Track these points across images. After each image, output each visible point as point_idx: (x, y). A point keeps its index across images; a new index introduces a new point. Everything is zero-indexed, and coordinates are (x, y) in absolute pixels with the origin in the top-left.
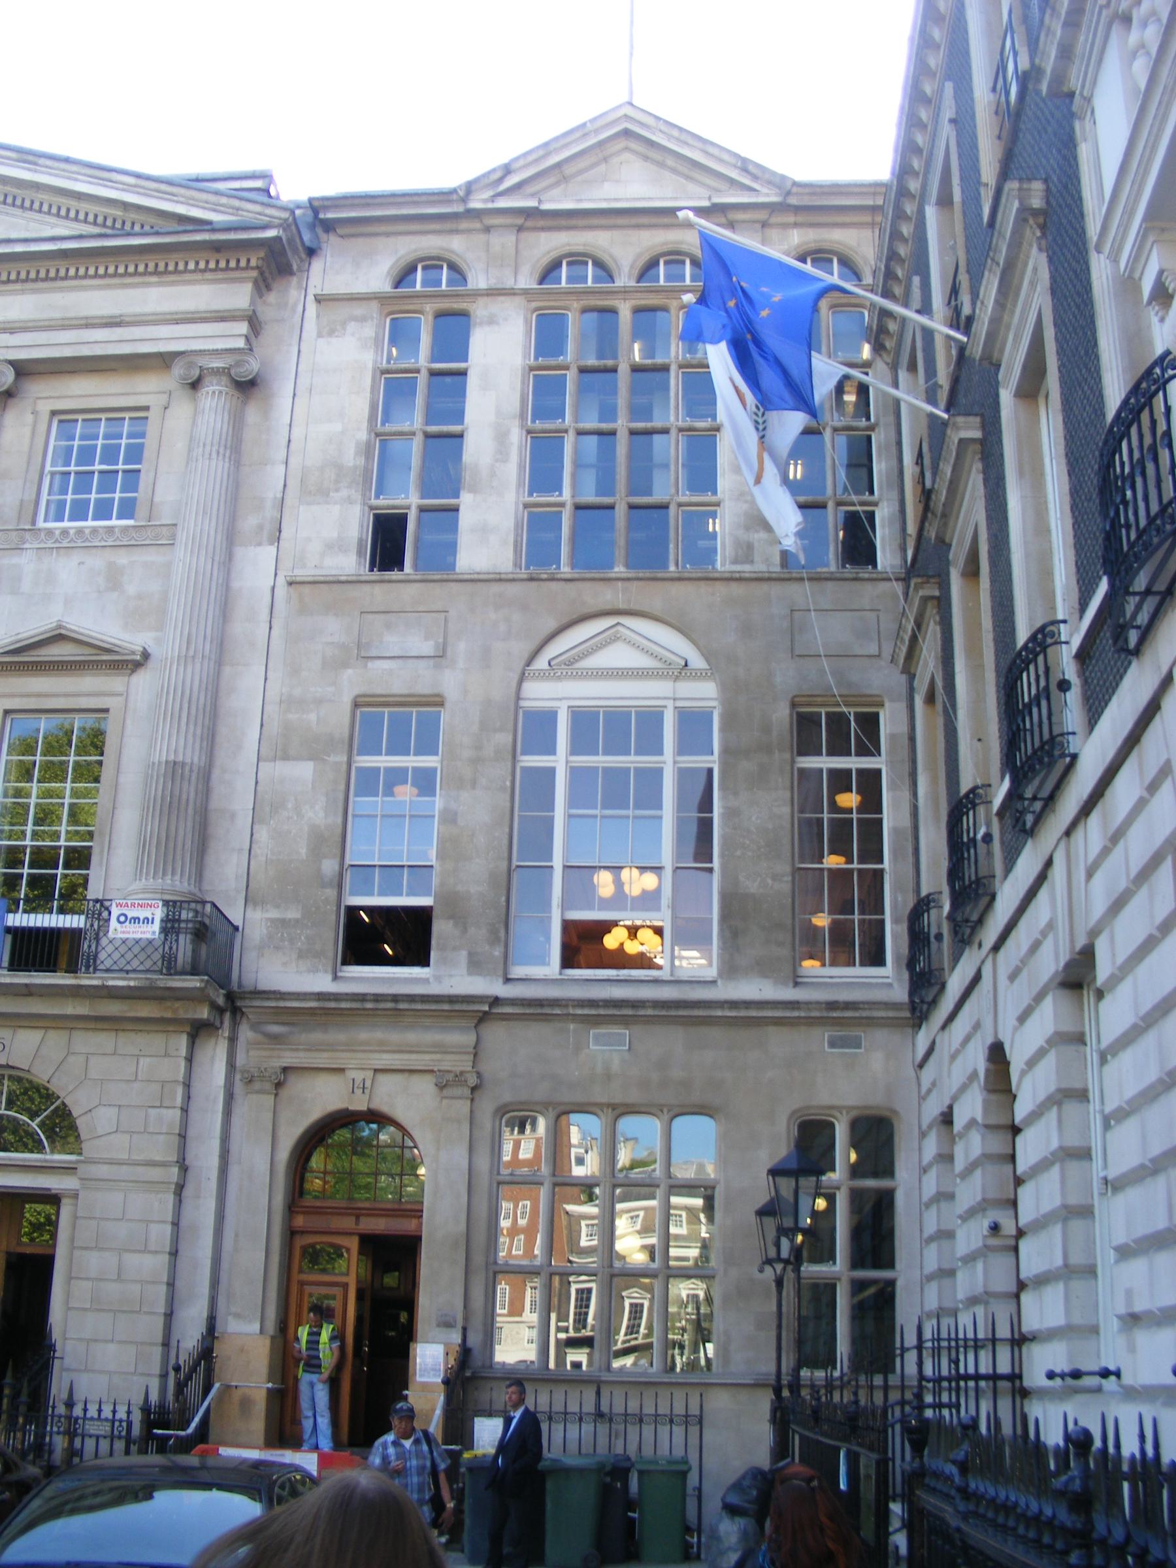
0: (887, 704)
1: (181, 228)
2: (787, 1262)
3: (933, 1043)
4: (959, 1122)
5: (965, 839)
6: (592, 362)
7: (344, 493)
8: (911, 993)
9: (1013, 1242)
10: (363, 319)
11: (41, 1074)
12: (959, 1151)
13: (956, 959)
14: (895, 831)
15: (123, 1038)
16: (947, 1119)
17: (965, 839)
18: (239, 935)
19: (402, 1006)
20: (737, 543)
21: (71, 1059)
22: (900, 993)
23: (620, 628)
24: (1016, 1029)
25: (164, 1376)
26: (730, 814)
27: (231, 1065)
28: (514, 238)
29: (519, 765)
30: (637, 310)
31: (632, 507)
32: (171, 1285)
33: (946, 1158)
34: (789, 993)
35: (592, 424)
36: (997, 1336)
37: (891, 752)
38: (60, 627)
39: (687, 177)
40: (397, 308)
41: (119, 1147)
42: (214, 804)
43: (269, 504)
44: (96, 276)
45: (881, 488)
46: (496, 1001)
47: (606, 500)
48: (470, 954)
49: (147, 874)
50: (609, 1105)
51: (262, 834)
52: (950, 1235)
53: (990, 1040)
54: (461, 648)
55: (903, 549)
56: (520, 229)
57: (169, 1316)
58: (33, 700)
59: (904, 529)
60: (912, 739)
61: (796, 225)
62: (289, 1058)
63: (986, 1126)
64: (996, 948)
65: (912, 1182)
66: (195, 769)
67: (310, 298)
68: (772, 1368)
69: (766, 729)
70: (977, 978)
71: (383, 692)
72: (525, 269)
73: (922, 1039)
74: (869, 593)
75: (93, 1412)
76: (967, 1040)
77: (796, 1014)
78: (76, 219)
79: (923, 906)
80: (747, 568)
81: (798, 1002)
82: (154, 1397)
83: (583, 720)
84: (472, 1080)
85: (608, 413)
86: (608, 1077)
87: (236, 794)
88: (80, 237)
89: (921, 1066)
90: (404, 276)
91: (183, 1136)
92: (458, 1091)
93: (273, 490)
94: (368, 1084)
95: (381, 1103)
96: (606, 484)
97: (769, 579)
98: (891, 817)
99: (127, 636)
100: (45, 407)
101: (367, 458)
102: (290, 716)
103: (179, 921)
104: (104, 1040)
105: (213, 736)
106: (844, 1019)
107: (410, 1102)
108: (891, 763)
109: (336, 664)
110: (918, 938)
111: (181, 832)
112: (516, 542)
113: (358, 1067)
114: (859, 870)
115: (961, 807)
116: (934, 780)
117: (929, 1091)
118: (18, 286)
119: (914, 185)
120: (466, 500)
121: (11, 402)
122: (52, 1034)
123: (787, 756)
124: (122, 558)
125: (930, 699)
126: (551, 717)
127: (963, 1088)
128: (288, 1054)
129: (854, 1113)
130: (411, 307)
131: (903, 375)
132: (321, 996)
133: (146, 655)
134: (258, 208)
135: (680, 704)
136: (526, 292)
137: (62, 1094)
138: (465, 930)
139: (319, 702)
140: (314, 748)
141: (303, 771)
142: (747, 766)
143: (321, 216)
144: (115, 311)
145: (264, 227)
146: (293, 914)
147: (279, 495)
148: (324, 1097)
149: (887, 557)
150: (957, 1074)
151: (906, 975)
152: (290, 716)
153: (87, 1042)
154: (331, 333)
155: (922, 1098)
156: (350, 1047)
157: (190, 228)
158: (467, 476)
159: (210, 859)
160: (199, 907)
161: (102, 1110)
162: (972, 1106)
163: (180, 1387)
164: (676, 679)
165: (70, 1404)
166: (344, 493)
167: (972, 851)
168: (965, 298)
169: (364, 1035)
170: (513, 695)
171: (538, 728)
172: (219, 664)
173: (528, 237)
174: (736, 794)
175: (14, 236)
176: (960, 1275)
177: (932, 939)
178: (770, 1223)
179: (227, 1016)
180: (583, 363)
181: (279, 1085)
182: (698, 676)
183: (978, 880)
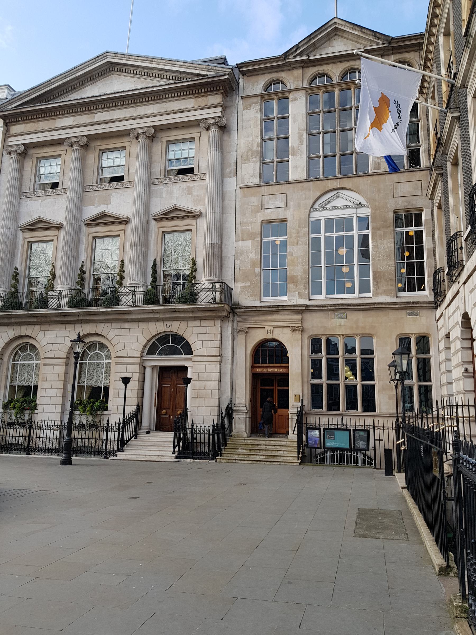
0: (424, 210)
1: (198, 78)
2: (398, 380)
3: (442, 313)
4: (452, 337)
5: (454, 249)
6: (327, 109)
7: (254, 159)
8: (434, 299)
9: (472, 375)
10: (256, 103)
11: (180, 333)
12: (452, 346)
13: (450, 287)
14: (428, 249)
15: (202, 322)
16: (448, 336)
17: (454, 249)
18: (233, 291)
19: (279, 309)
20: (375, 163)
21: (188, 328)
22: (431, 299)
23: (339, 194)
24: (472, 308)
25: (219, 416)
26: (374, 247)
27: (233, 328)
28: (301, 71)
29: (310, 237)
30: (341, 90)
31: (341, 155)
32: (219, 390)
33: (448, 348)
34: (395, 300)
35: (328, 129)
36: (470, 404)
37: (426, 224)
38: (175, 206)
39: (356, 42)
40: (266, 98)
41: (202, 352)
42: (223, 255)
43: (232, 165)
44: (175, 96)
45: (422, 140)
46: (307, 306)
47: (333, 154)
48: (299, 293)
49: (211, 275)
50: (341, 335)
51: (238, 262)
52: (450, 372)
53: (463, 312)
54: (291, 204)
55: (429, 160)
56: (303, 67)
57: (219, 399)
58: (165, 228)
59: (429, 153)
60: (433, 220)
61: (393, 54)
62: (249, 325)
63: (462, 339)
64: (465, 283)
65: (436, 355)
66: (217, 245)
67: (240, 98)
68: (395, 411)
69: (386, 221)
70: (458, 292)
71: (268, 219)
72: (305, 81)
73: (438, 312)
74: (418, 175)
75: (199, 427)
76: (454, 312)
77: (397, 306)
78: (167, 79)
79: (437, 272)
80: (378, 171)
81: (398, 302)
82: (216, 422)
83: (329, 222)
84: (301, 329)
85: (333, 126)
86: (341, 326)
87: (229, 252)
88: (168, 84)
89: (438, 321)
90: (267, 86)
91: (221, 348)
92: (297, 332)
93: (233, 161)
94: (271, 331)
95: (276, 337)
96: (333, 149)
97: (386, 174)
98: (426, 244)
99: (195, 208)
100: (164, 140)
101: (260, 148)
102: (243, 228)
103: (216, 288)
104: (197, 323)
105: (222, 235)
106: (413, 308)
107: (284, 336)
108: (426, 228)
109: (255, 212)
110: (436, 282)
111: (215, 263)
112: (306, 170)
113: (269, 326)
114: (416, 262)
115: (451, 239)
116: (440, 232)
117: (441, 328)
118: (152, 102)
119: (434, 30)
120: (291, 157)
121: (154, 139)
122: (182, 322)
123: (393, 228)
124: (191, 184)
125: (439, 207)
126: (319, 221)
127: (454, 327)
128: (249, 324)
129: (417, 335)
130: (271, 98)
131: (430, 100)
132: (256, 307)
133: (201, 213)
134: (221, 69)
135: (358, 215)
136: (306, 89)
137: (186, 338)
138: (297, 287)
139: (251, 223)
140: (251, 236)
141: (247, 245)
142: (379, 232)
143: (241, 70)
144: (181, 108)
145: (224, 75)
146: (248, 284)
147: (235, 162)
148: (259, 336)
149: (424, 163)
150: (450, 324)
151: (433, 293)
152: (243, 228)
153: (192, 323)
154: (247, 109)
155: (438, 331)
156: (265, 321)
157: (201, 78)
158: (291, 150)
159: (223, 270)
160: (221, 284)
161: (198, 342)
162: (457, 332)
163: (223, 419)
164: (357, 208)
165: (193, 426)
166: (254, 159)
167: (456, 253)
168: (453, 67)
169: (269, 317)
170: (308, 217)
171: (315, 227)
172: (222, 214)
173: (306, 70)
174: (376, 241)
175: (148, 86)
176: (454, 384)
177: (442, 282)
178: (392, 368)
179: (231, 314)
180: (324, 110)
181: (247, 332)
182: (365, 206)
183: (458, 262)
